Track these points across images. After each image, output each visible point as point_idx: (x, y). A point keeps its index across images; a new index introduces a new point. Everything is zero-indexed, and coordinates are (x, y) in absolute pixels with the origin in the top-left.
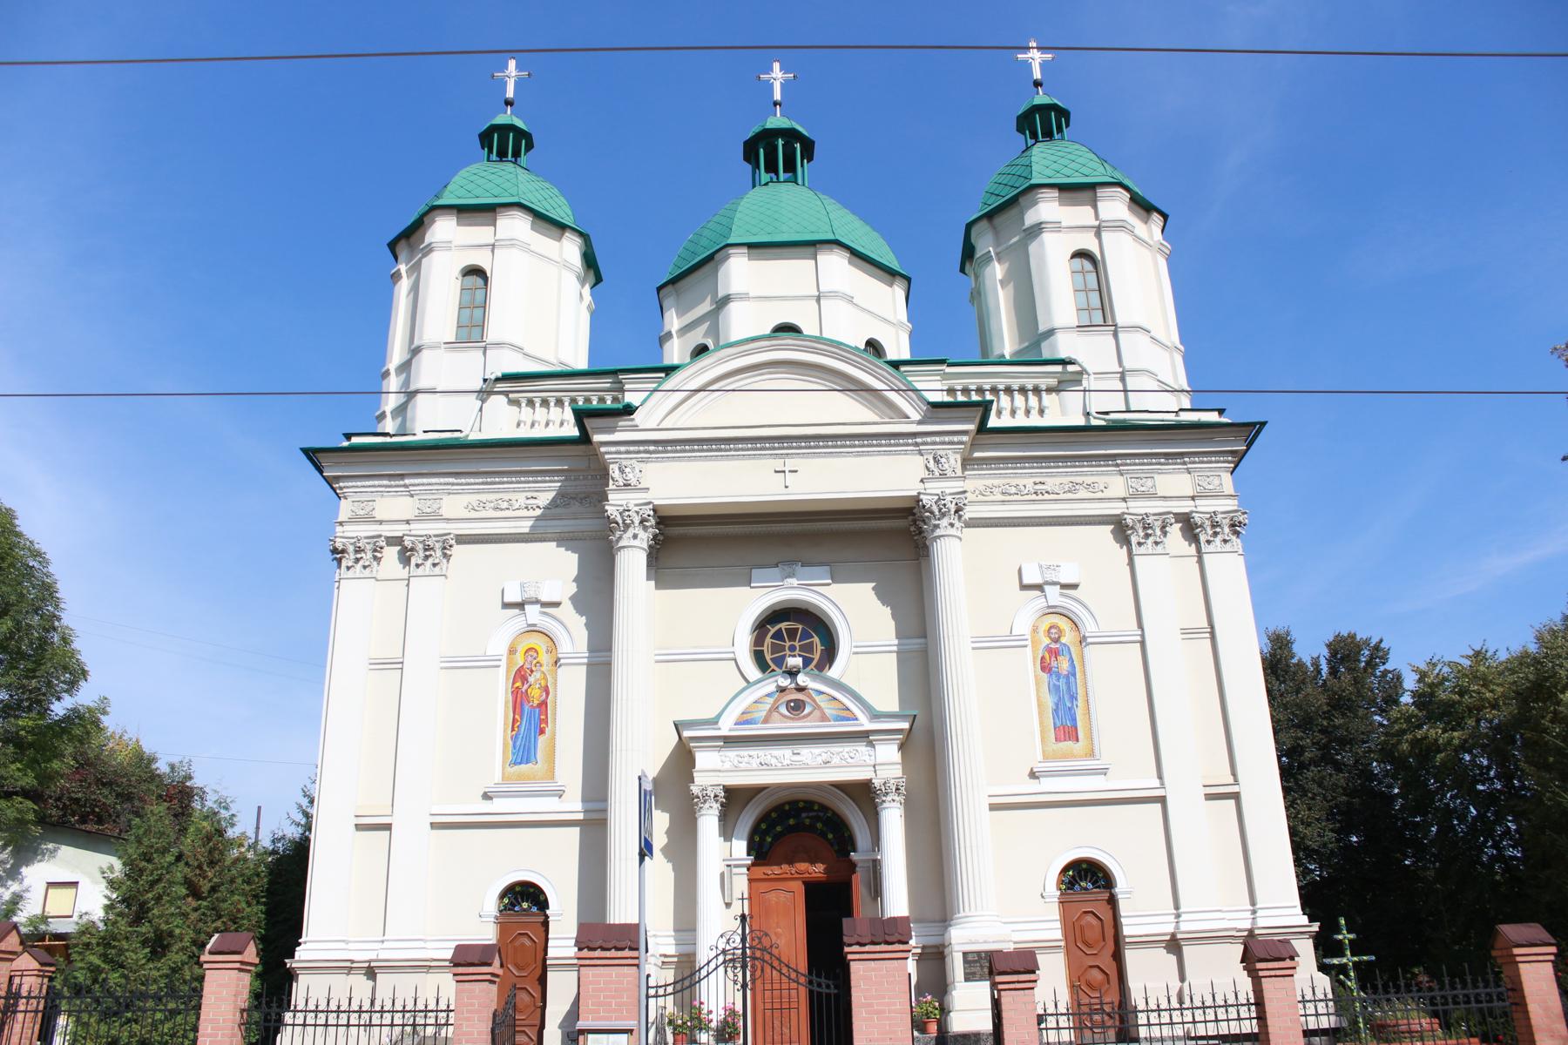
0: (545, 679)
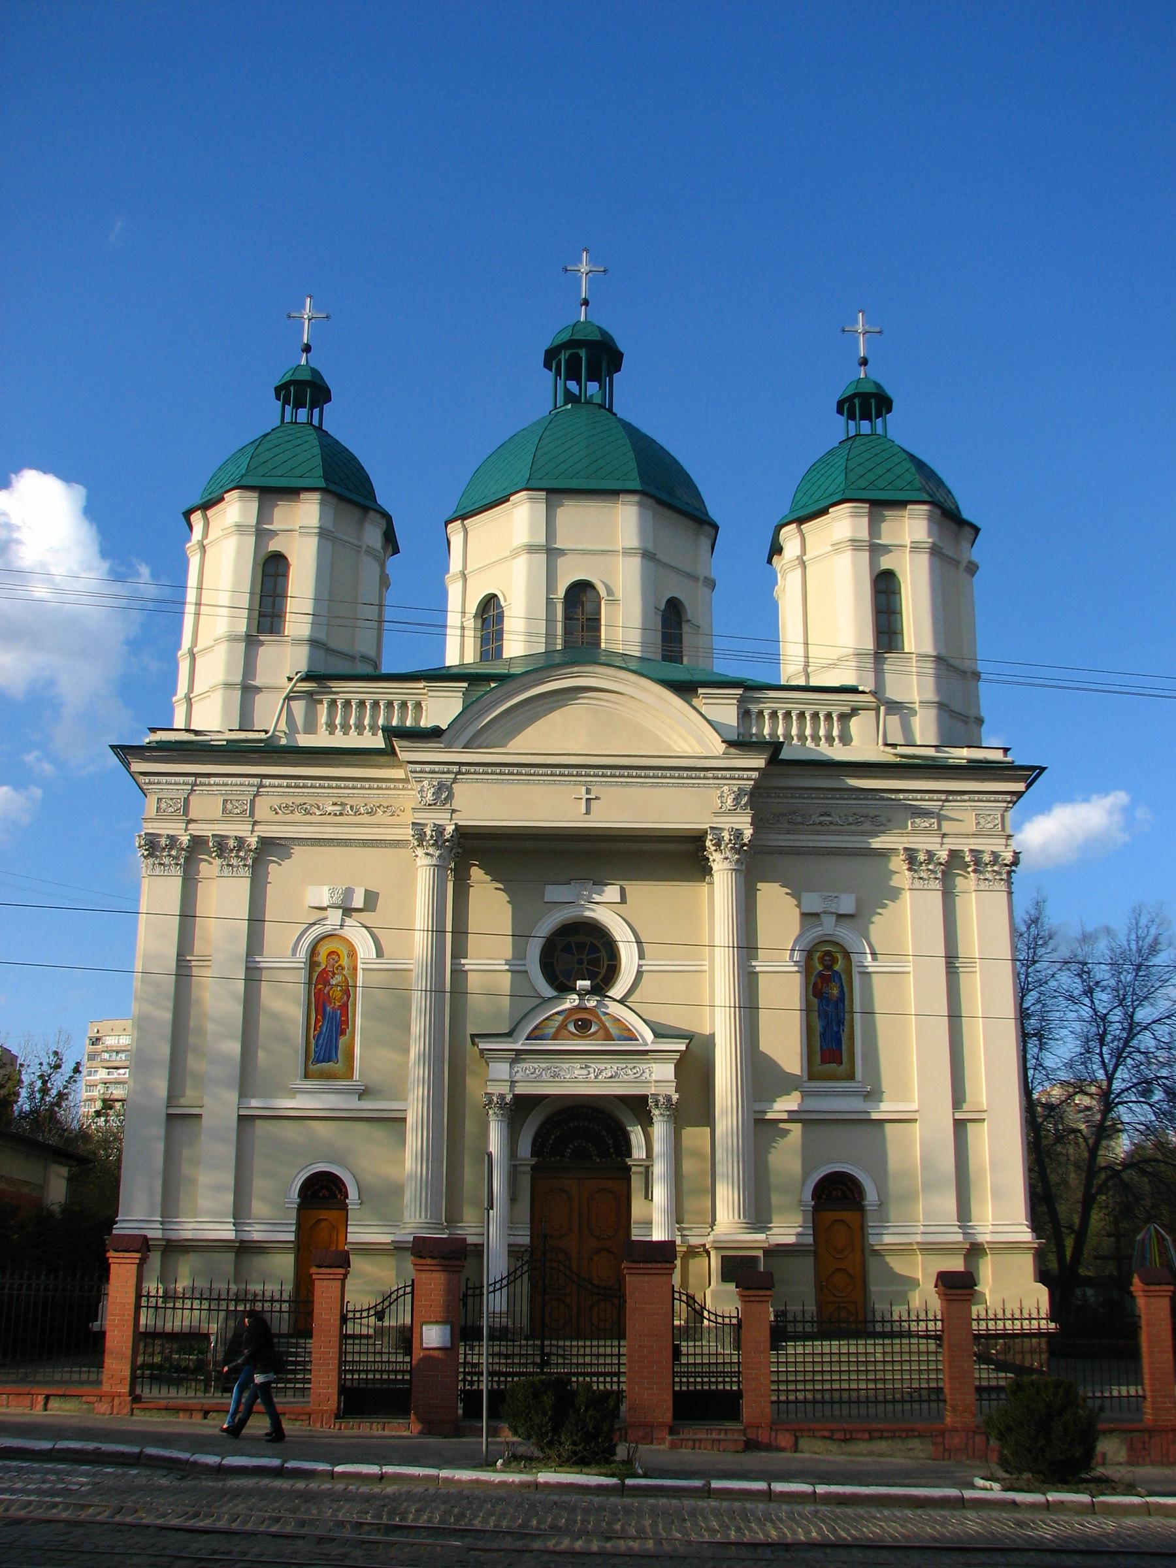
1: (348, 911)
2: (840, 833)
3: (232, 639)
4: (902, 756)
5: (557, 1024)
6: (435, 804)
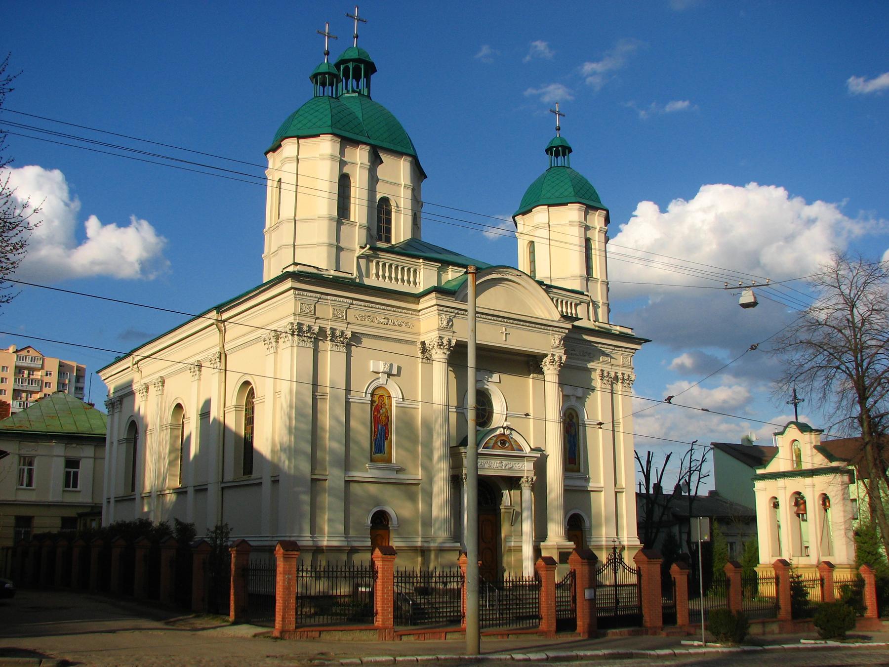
0: (387, 412)
1: (389, 375)
2: (578, 359)
3: (331, 219)
4: (599, 327)
5: (494, 441)
6: (447, 328)
